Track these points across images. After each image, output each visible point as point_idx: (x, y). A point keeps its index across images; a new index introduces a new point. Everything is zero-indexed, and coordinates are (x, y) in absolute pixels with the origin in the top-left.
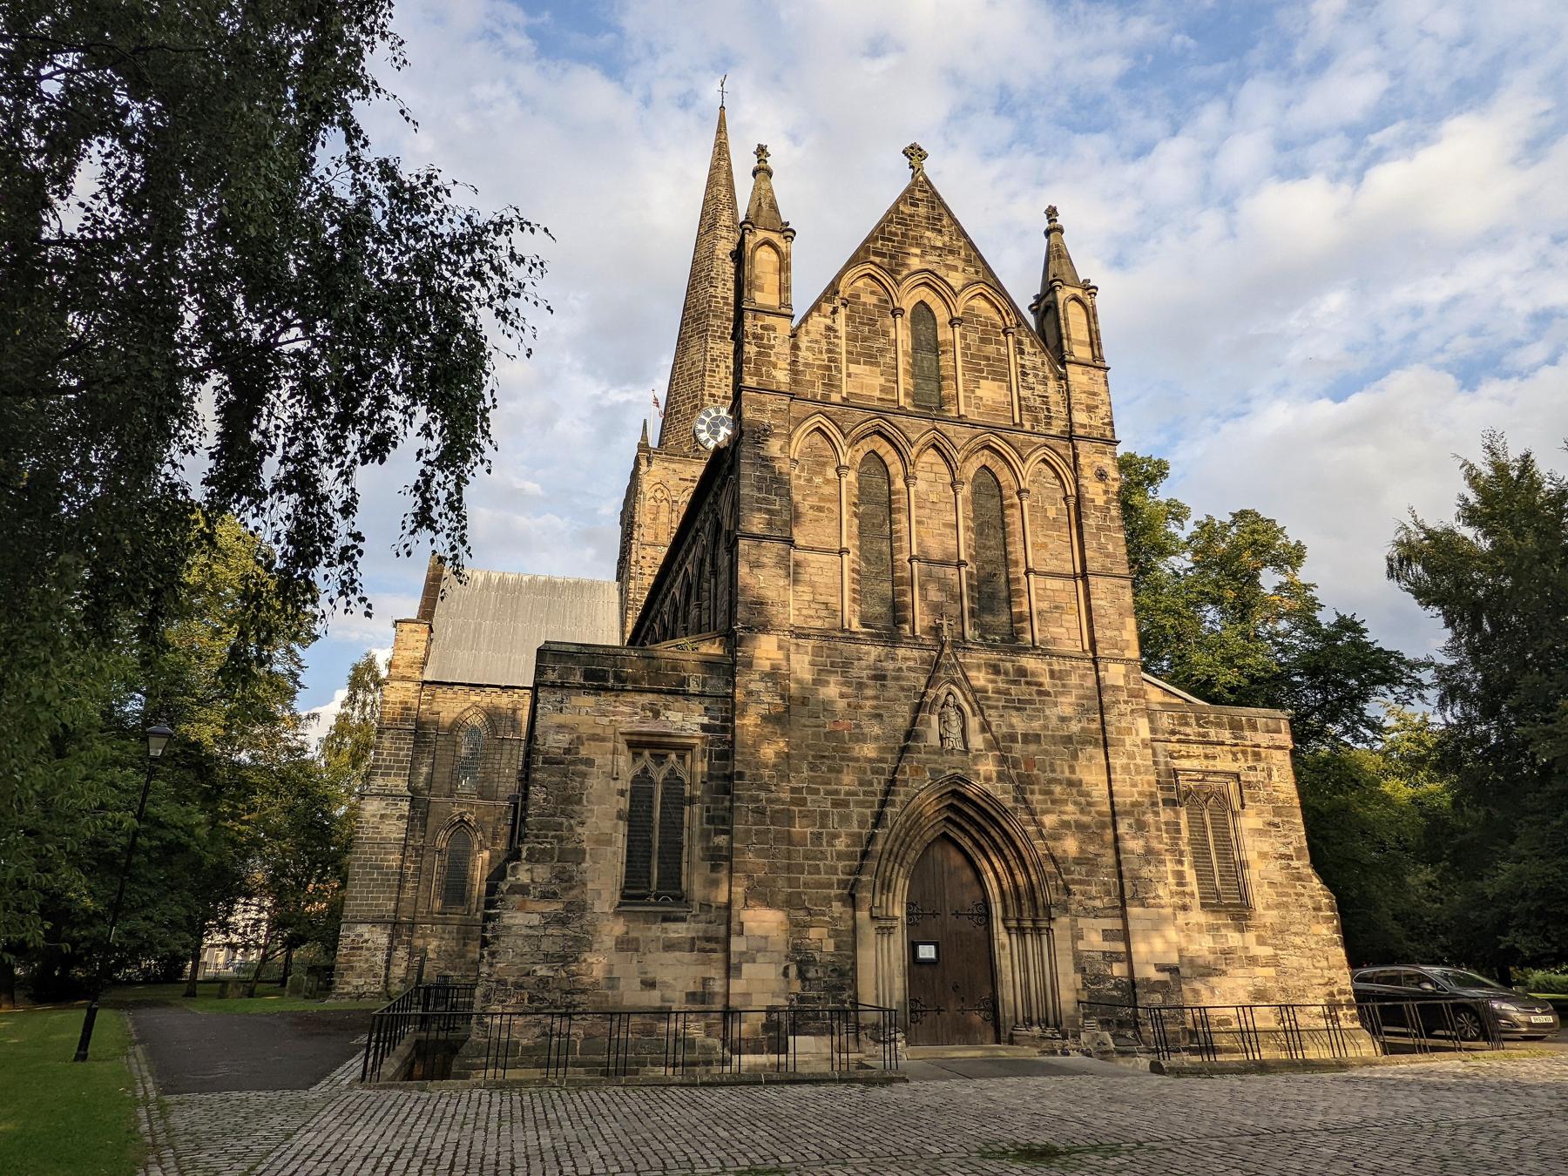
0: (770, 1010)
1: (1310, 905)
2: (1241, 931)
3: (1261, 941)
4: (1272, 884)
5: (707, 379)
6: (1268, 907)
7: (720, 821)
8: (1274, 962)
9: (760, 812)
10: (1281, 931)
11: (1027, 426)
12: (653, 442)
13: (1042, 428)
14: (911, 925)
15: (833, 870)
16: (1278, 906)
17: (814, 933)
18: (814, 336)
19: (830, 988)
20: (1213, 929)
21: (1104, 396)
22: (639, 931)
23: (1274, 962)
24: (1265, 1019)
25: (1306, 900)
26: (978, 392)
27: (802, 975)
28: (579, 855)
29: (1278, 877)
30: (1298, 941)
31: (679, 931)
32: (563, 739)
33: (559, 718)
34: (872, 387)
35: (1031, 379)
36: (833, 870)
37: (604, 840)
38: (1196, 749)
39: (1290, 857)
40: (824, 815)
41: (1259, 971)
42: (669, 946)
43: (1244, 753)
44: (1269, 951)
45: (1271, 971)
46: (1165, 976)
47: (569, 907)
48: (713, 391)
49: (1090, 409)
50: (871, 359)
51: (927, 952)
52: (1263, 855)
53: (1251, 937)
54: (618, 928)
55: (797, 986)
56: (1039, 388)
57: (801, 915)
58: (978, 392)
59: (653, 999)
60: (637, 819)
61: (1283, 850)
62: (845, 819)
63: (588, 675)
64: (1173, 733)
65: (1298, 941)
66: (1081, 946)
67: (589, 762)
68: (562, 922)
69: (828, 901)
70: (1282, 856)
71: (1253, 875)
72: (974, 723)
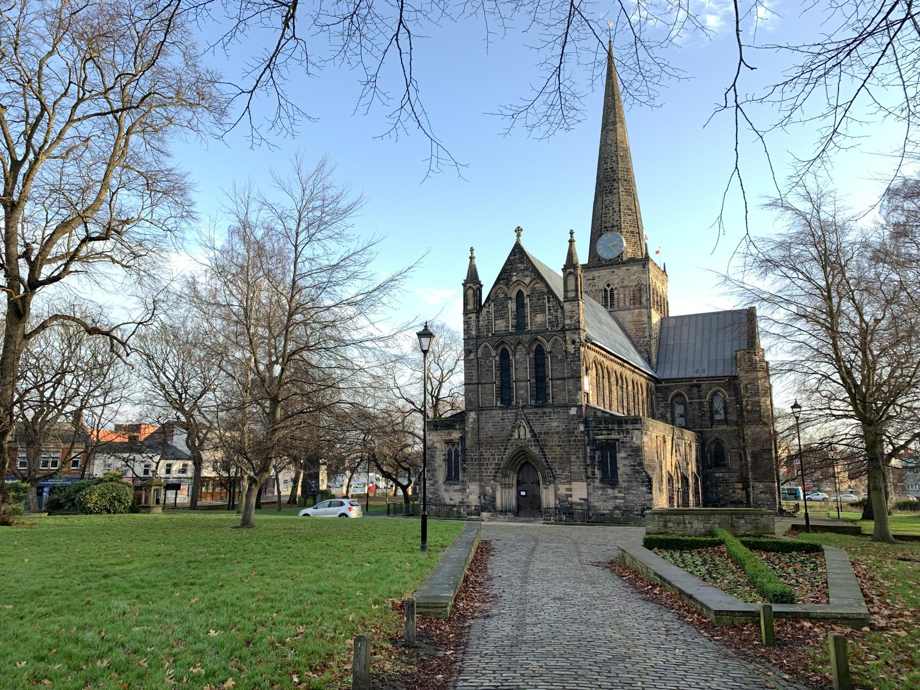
0: (476, 506)
1: (640, 480)
2: (613, 489)
3: (619, 492)
4: (626, 474)
5: (604, 219)
6: (624, 482)
7: (464, 461)
8: (624, 498)
9: (472, 459)
10: (626, 489)
11: (550, 329)
12: (583, 257)
13: (555, 329)
14: (518, 486)
15: (491, 472)
16: (628, 482)
17: (487, 488)
18: (484, 316)
19: (491, 501)
20: (603, 488)
21: (577, 311)
22: (448, 487)
23: (624, 498)
24: (618, 514)
25: (639, 479)
26: (536, 320)
27: (484, 498)
28: (435, 470)
29: (629, 472)
30: (634, 492)
31: (456, 487)
32: (431, 442)
33: (430, 438)
34: (502, 327)
35: (552, 311)
36: (491, 472)
37: (440, 466)
38: (605, 432)
39: (635, 466)
40: (489, 458)
41: (618, 501)
42: (455, 491)
43: (623, 432)
44: (623, 495)
45: (622, 501)
46: (582, 501)
47: (434, 482)
48: (606, 225)
49: (571, 318)
50: (502, 317)
51: (523, 493)
52: (625, 465)
53: (616, 491)
54: (444, 487)
55: (483, 501)
56: (555, 314)
57: (484, 484)
58: (536, 320)
59: (452, 503)
60: (448, 461)
61: (633, 463)
62: (494, 459)
63: (434, 427)
64: (596, 427)
65: (634, 492)
66: (559, 492)
67: (436, 448)
68: (433, 485)
69: (490, 480)
70: (632, 466)
71: (620, 472)
72: (527, 430)
